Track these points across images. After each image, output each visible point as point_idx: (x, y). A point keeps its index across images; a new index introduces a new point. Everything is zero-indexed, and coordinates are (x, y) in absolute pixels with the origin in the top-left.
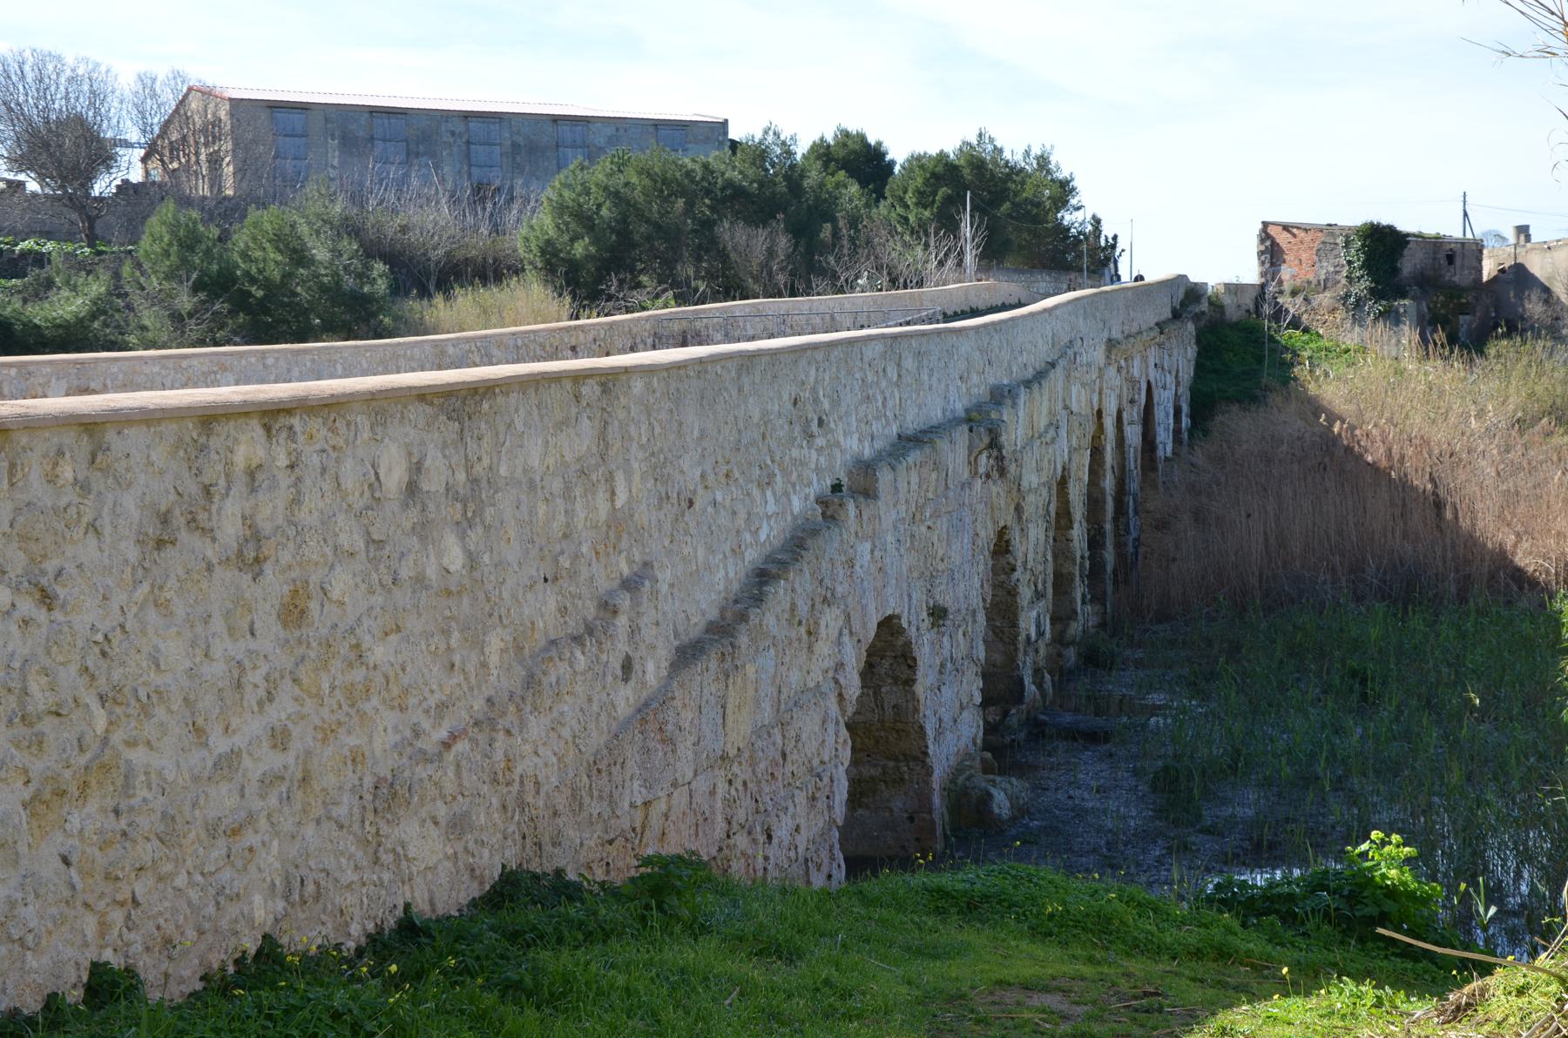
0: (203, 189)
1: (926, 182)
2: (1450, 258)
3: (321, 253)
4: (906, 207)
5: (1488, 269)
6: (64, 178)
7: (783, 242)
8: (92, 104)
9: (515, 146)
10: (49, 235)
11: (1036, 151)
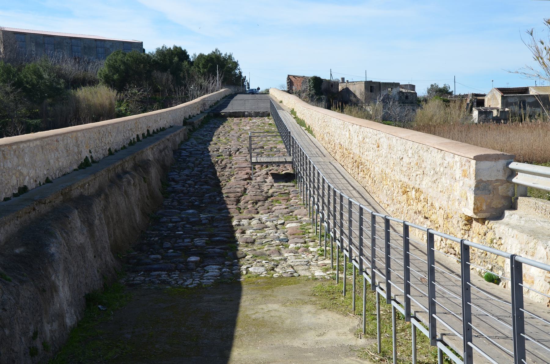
2: (332, 86)
3: (46, 76)
4: (200, 68)
5: (340, 88)
7: (171, 77)
9: (84, 47)
11: (228, 54)
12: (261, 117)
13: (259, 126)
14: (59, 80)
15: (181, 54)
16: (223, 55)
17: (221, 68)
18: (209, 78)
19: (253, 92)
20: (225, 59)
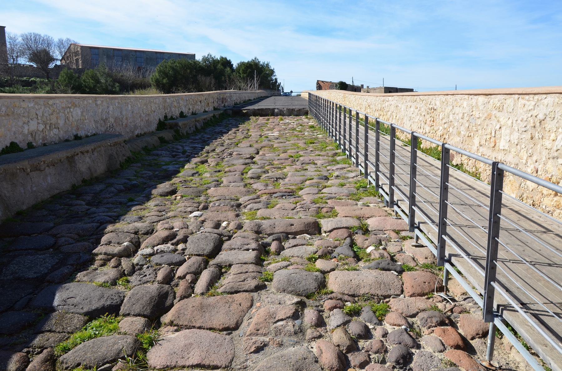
0: (74, 67)
1: (245, 68)
3: (103, 81)
6: (41, 63)
7: (213, 81)
8: (48, 46)
9: (147, 58)
10: (38, 77)
11: (266, 63)
12: (297, 116)
13: (294, 129)
14: (114, 84)
15: (226, 63)
16: (261, 63)
17: (259, 75)
18: (247, 81)
19: (287, 95)
20: (263, 66)
